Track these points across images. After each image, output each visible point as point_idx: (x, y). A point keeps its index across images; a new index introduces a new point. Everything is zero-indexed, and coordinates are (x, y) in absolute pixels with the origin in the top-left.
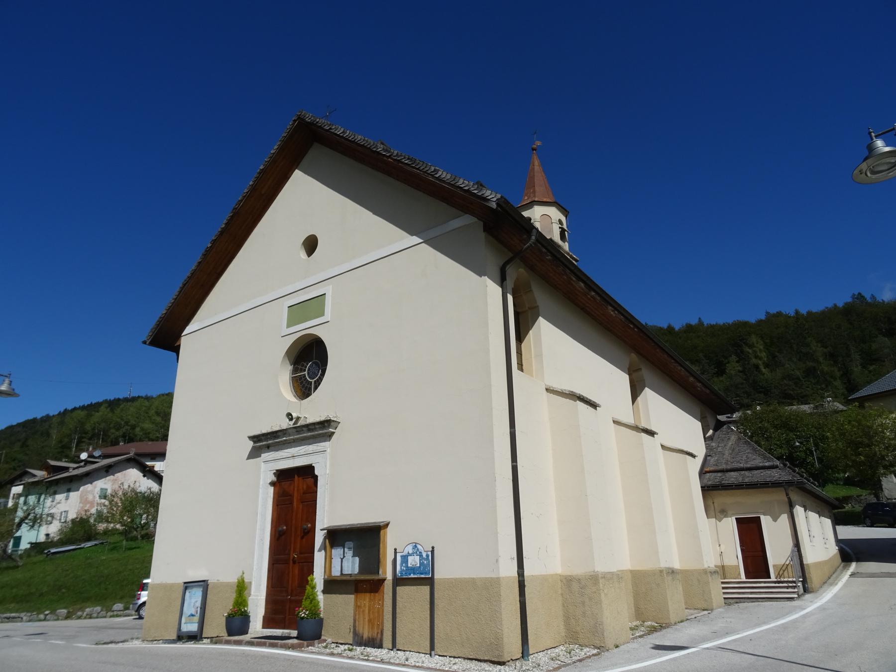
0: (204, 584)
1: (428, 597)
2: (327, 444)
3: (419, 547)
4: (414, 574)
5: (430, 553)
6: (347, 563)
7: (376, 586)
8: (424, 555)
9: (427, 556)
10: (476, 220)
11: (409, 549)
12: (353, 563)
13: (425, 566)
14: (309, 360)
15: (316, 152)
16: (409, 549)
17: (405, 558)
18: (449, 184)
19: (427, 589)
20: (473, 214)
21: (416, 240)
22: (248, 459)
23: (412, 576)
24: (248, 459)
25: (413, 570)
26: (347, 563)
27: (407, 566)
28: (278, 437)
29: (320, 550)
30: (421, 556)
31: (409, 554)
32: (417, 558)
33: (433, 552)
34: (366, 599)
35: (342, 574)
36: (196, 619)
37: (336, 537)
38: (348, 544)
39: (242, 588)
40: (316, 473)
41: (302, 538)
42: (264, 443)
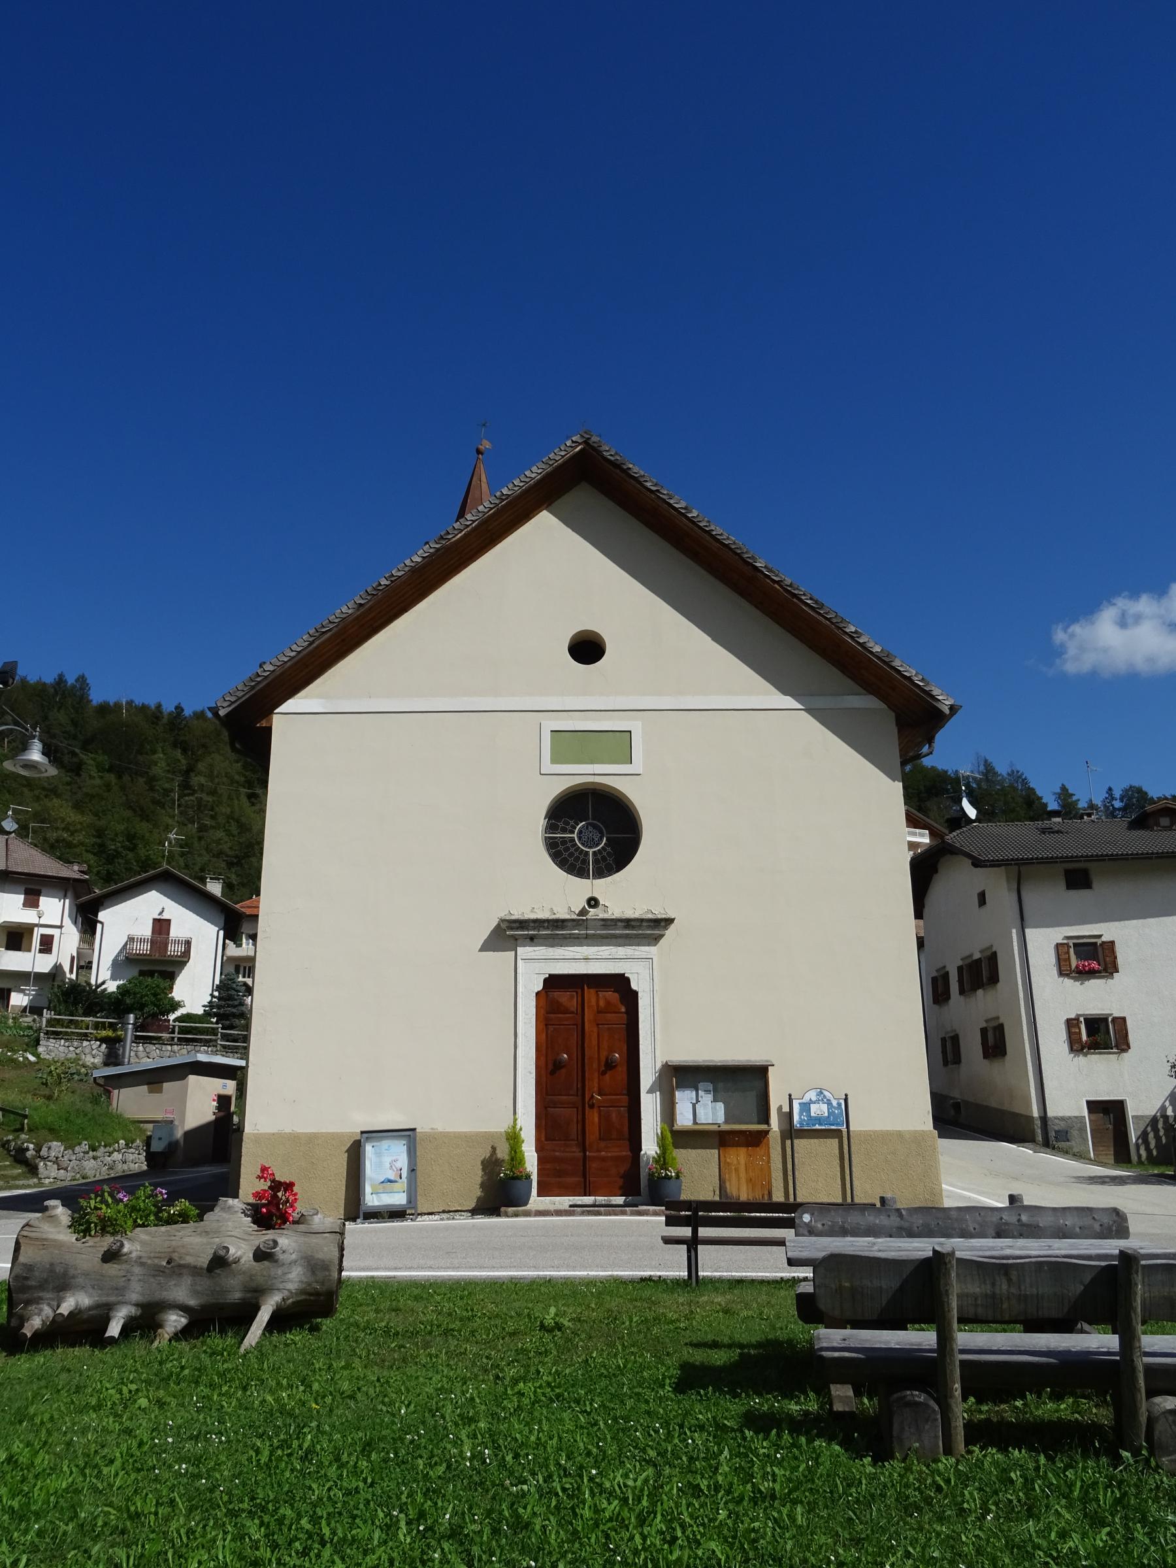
0: (408, 1134)
1: (837, 1152)
2: (651, 951)
3: (826, 1093)
4: (820, 1124)
5: (843, 1102)
6: (702, 1109)
7: (756, 1140)
8: (835, 1103)
9: (839, 1105)
10: (884, 706)
11: (812, 1095)
12: (714, 1109)
13: (836, 1117)
14: (595, 827)
15: (581, 496)
16: (812, 1095)
17: (806, 1107)
18: (879, 658)
19: (835, 1142)
20: (883, 698)
21: (789, 702)
22: (481, 950)
23: (817, 1127)
24: (481, 950)
25: (819, 1120)
26: (702, 1109)
27: (809, 1115)
28: (563, 928)
29: (650, 1091)
30: (829, 1103)
31: (811, 1102)
32: (824, 1107)
33: (846, 1100)
34: (739, 1156)
35: (695, 1122)
36: (403, 1184)
37: (681, 1076)
38: (701, 1085)
39: (514, 1138)
40: (634, 986)
41: (604, 1073)
42: (511, 934)
